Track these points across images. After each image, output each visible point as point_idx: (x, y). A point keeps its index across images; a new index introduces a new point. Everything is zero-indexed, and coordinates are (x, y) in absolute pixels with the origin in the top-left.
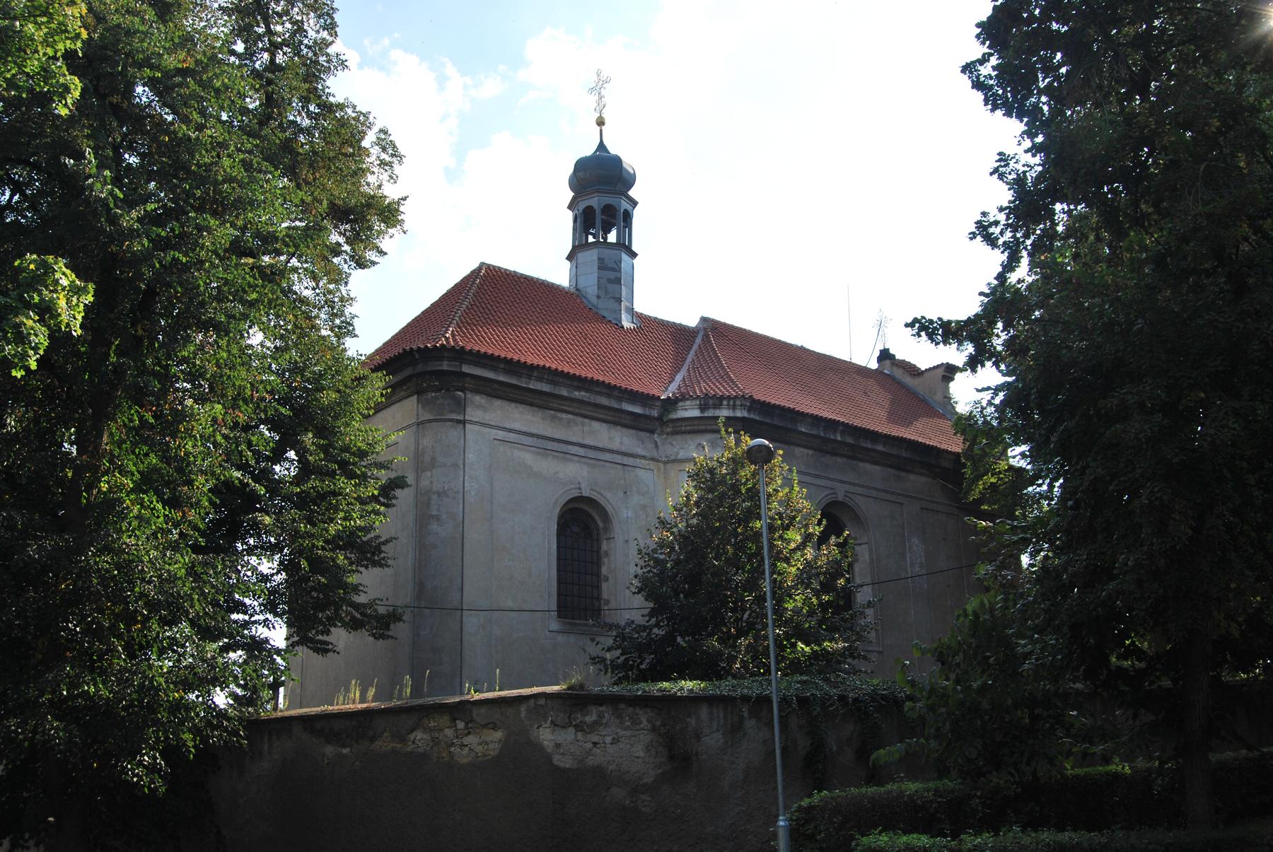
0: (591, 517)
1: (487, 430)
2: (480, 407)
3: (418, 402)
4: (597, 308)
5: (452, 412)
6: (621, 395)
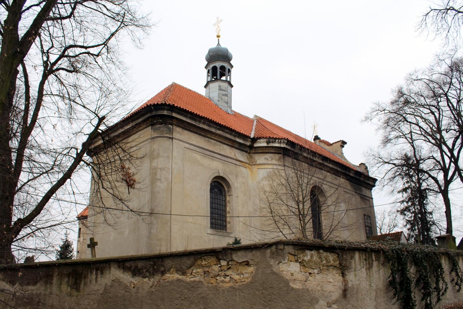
0: (222, 186)
1: (182, 143)
2: (179, 133)
3: (152, 129)
4: (218, 105)
5: (167, 133)
6: (235, 134)
